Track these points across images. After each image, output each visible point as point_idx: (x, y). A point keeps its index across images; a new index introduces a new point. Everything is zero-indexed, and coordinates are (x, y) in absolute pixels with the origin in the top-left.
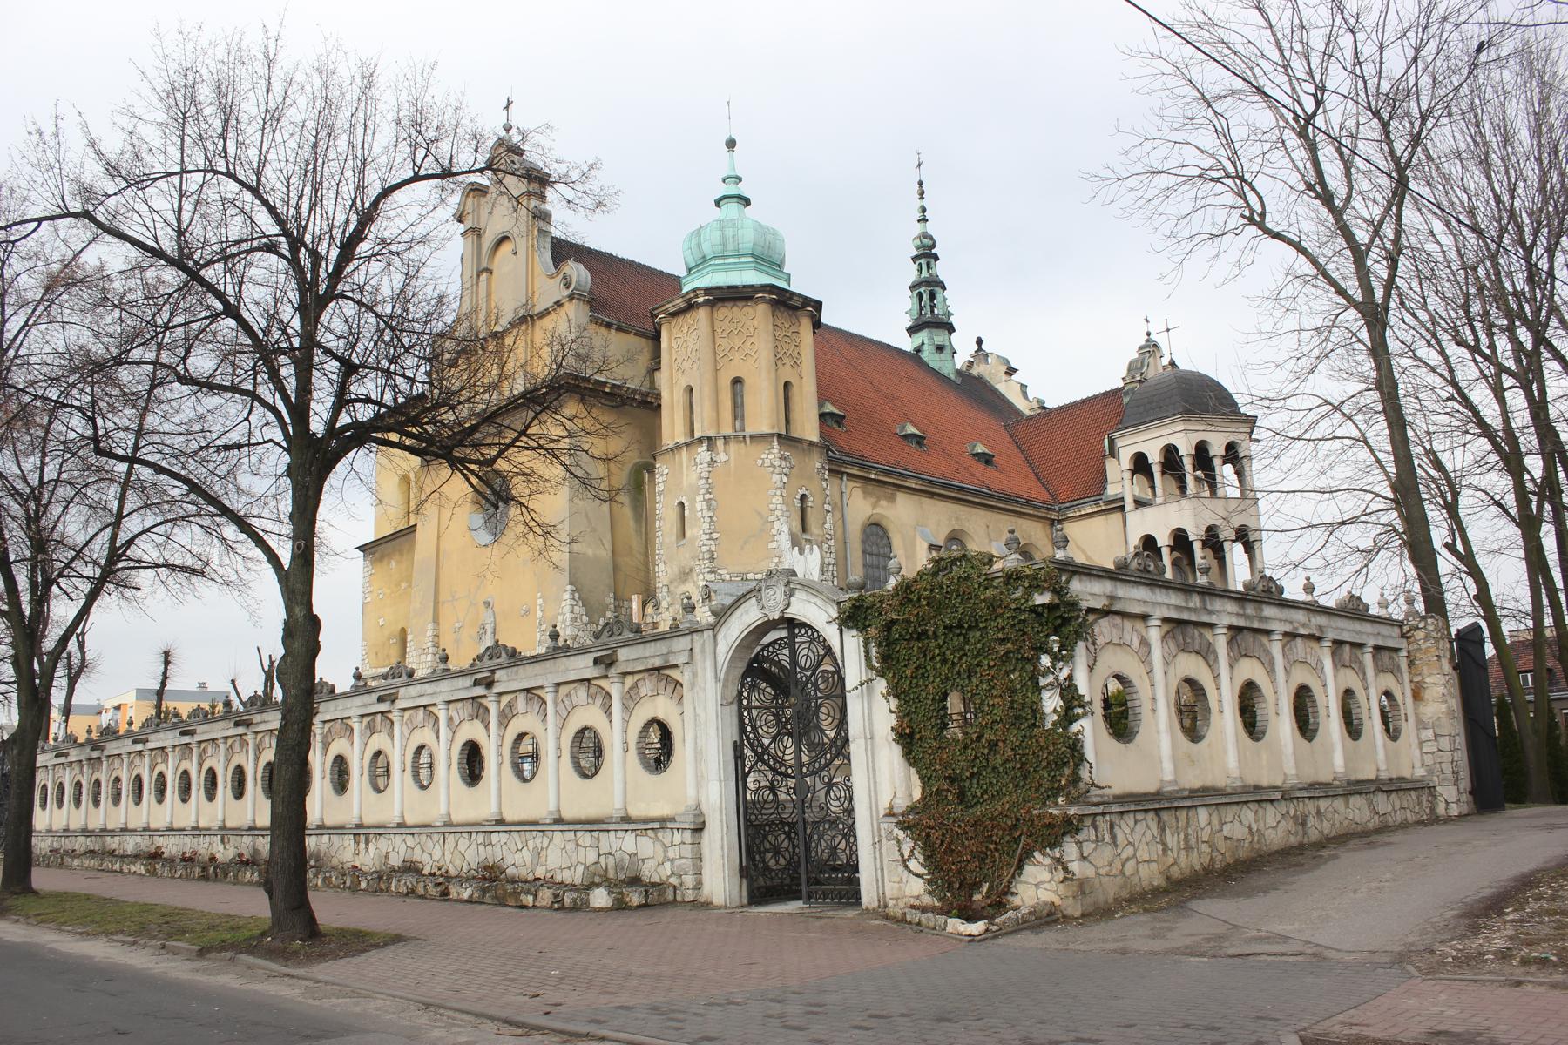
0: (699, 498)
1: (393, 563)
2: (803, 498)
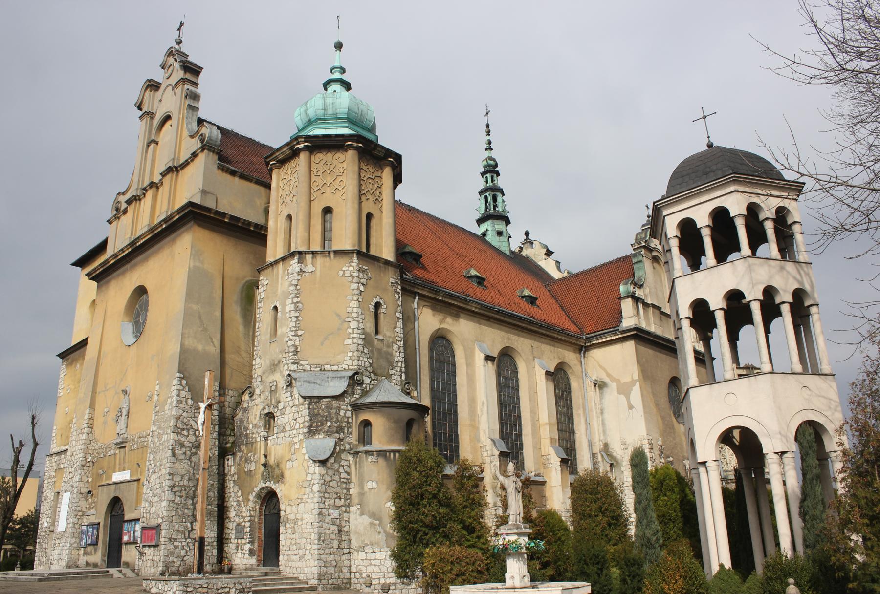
0: (289, 301)
1: (78, 365)
2: (378, 305)
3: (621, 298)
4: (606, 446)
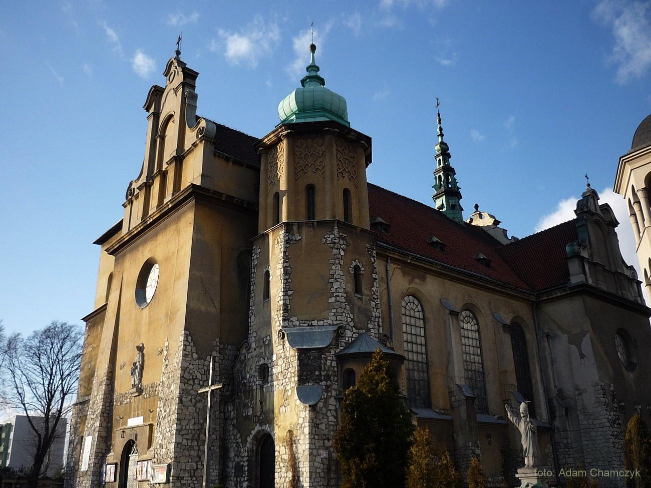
1: (99, 327)
3: (567, 259)
4: (560, 391)
